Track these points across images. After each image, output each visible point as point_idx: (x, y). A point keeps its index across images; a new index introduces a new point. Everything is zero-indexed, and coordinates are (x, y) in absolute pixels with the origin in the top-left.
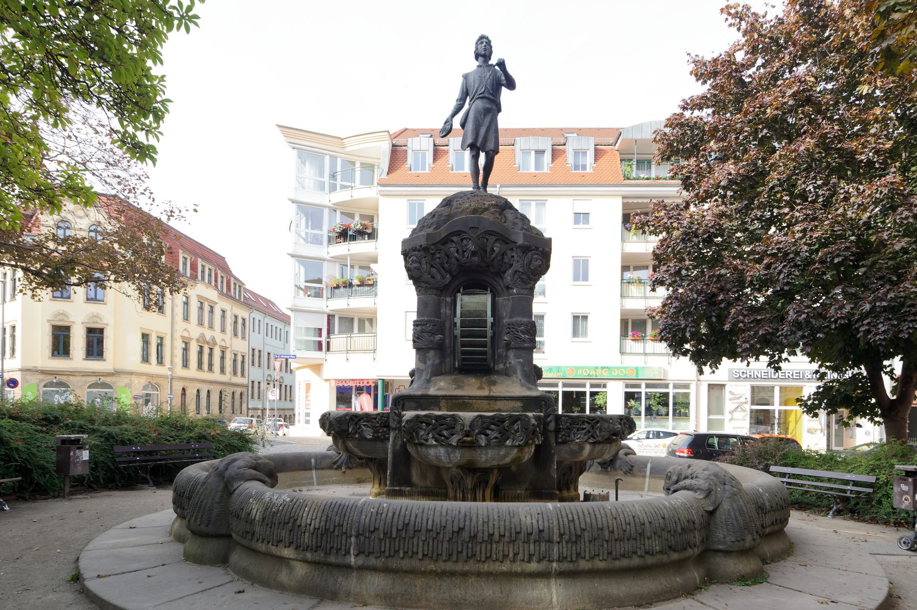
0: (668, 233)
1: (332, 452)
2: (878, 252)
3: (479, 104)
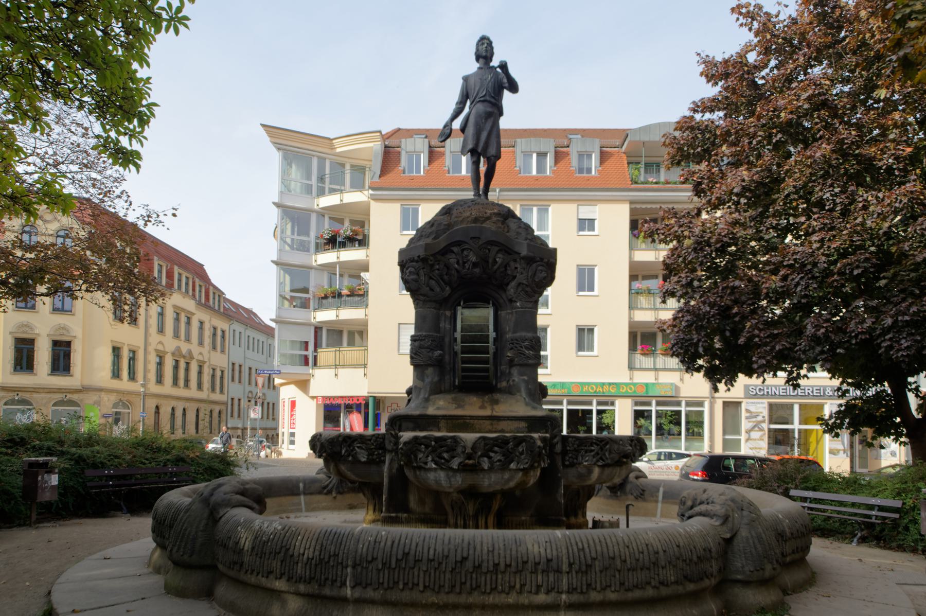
0: (679, 242)
1: (322, 476)
2: (899, 263)
3: (480, 107)
